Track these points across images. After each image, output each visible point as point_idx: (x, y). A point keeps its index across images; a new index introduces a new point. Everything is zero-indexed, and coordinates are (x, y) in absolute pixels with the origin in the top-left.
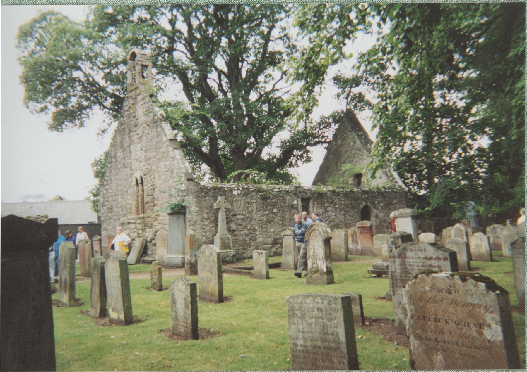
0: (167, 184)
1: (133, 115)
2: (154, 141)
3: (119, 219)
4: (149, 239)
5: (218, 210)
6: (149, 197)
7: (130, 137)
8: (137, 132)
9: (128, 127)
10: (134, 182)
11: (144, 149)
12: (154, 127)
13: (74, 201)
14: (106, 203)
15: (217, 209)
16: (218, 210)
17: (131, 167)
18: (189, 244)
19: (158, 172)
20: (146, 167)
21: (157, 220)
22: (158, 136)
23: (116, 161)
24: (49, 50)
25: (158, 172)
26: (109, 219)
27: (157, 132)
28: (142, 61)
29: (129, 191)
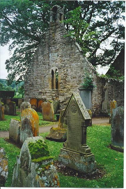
0: (78, 74)
1: (53, 38)
2: (69, 52)
3: (38, 90)
4: (61, 101)
5: (105, 89)
6: (62, 80)
7: (49, 50)
8: (55, 47)
9: (48, 44)
10: (50, 72)
11: (60, 55)
12: (69, 45)
13: (82, 140)
14: (28, 82)
15: (105, 89)
16: (105, 89)
17: (49, 65)
18: (124, 117)
19: (70, 68)
20: (60, 65)
21: (68, 92)
22: (72, 50)
23: (38, 61)
24: (14, 121)
25: (70, 68)
26: (31, 90)
27: (72, 48)
28: (60, 11)
29: (47, 76)
